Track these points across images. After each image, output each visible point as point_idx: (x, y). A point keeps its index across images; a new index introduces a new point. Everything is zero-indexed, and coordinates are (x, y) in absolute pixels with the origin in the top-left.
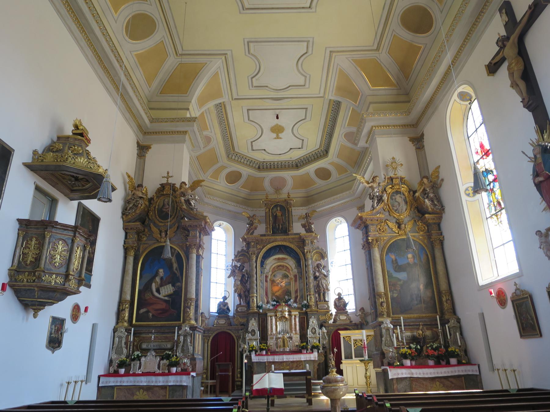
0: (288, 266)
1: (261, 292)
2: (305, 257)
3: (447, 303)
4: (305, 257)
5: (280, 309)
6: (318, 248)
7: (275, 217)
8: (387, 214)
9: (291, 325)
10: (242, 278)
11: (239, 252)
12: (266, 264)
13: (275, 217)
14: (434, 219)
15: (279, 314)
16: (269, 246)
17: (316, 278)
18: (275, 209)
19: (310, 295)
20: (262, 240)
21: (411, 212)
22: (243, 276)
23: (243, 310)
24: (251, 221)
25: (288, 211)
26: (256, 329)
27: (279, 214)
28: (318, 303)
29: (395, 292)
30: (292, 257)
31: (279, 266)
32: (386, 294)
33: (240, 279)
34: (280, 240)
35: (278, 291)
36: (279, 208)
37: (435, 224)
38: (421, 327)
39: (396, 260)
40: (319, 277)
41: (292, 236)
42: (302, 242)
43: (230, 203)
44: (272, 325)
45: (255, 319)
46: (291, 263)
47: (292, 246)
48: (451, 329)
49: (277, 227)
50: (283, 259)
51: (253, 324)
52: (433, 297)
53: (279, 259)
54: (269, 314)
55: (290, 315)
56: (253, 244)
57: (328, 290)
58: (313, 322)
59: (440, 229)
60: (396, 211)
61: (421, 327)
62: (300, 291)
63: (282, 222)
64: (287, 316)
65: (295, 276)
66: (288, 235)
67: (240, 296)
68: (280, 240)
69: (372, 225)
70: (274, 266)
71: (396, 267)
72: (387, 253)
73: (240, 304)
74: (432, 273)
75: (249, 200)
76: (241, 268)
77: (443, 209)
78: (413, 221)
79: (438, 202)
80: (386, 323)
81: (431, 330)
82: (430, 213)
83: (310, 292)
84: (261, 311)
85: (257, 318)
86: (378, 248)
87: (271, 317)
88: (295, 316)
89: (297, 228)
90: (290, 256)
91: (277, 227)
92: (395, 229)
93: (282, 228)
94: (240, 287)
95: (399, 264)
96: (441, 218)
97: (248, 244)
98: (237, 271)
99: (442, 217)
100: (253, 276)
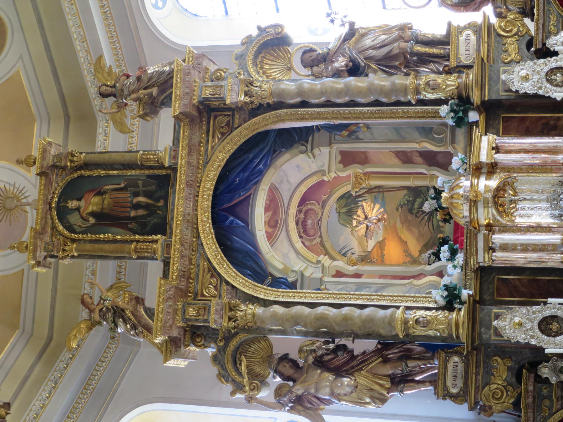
0: (303, 189)
1: (395, 292)
2: (271, 107)
4: (271, 107)
5: (462, 213)
6: (241, 57)
7: (104, 219)
9: (531, 168)
10: (330, 370)
11: (223, 376)
12: (286, 270)
13: (104, 219)
15: (484, 216)
16: (212, 249)
17: (354, 70)
18: (74, 219)
19: (417, 91)
20: (186, 275)
22: (320, 363)
23: (461, 367)
24: (103, 315)
25: (86, 166)
26: (539, 312)
27: (92, 204)
28: (453, 63)
30: (267, 166)
31: (302, 225)
33: (331, 377)
34: (192, 205)
35: (404, 243)
36: (72, 204)
40: (352, 60)
41: (182, 152)
42: (208, 114)
43: (36, 404)
44: (526, 248)
45: (497, 317)
46: (291, 172)
47: (220, 158)
49: (141, 212)
50: (273, 205)
51: (517, 324)
53: (273, 224)
54: (482, 258)
55: (492, 168)
56: (192, 312)
57: (403, 28)
58: (526, 78)
62: (403, 140)
63: (127, 195)
64: (494, 183)
65: (348, 159)
66: (174, 169)
67: (400, 382)
68: (192, 205)
70: (299, 245)
73: (432, 381)
75: (50, 339)
76: (288, 370)
83: (405, 90)
84: (465, 293)
85: (495, 310)
87: (493, 250)
88: (497, 149)
89: (159, 137)
90: (261, 173)
91: (141, 212)
93: (147, 194)
94: (362, 379)
97: (196, 333)
98: (299, 390)
100: (322, 318)
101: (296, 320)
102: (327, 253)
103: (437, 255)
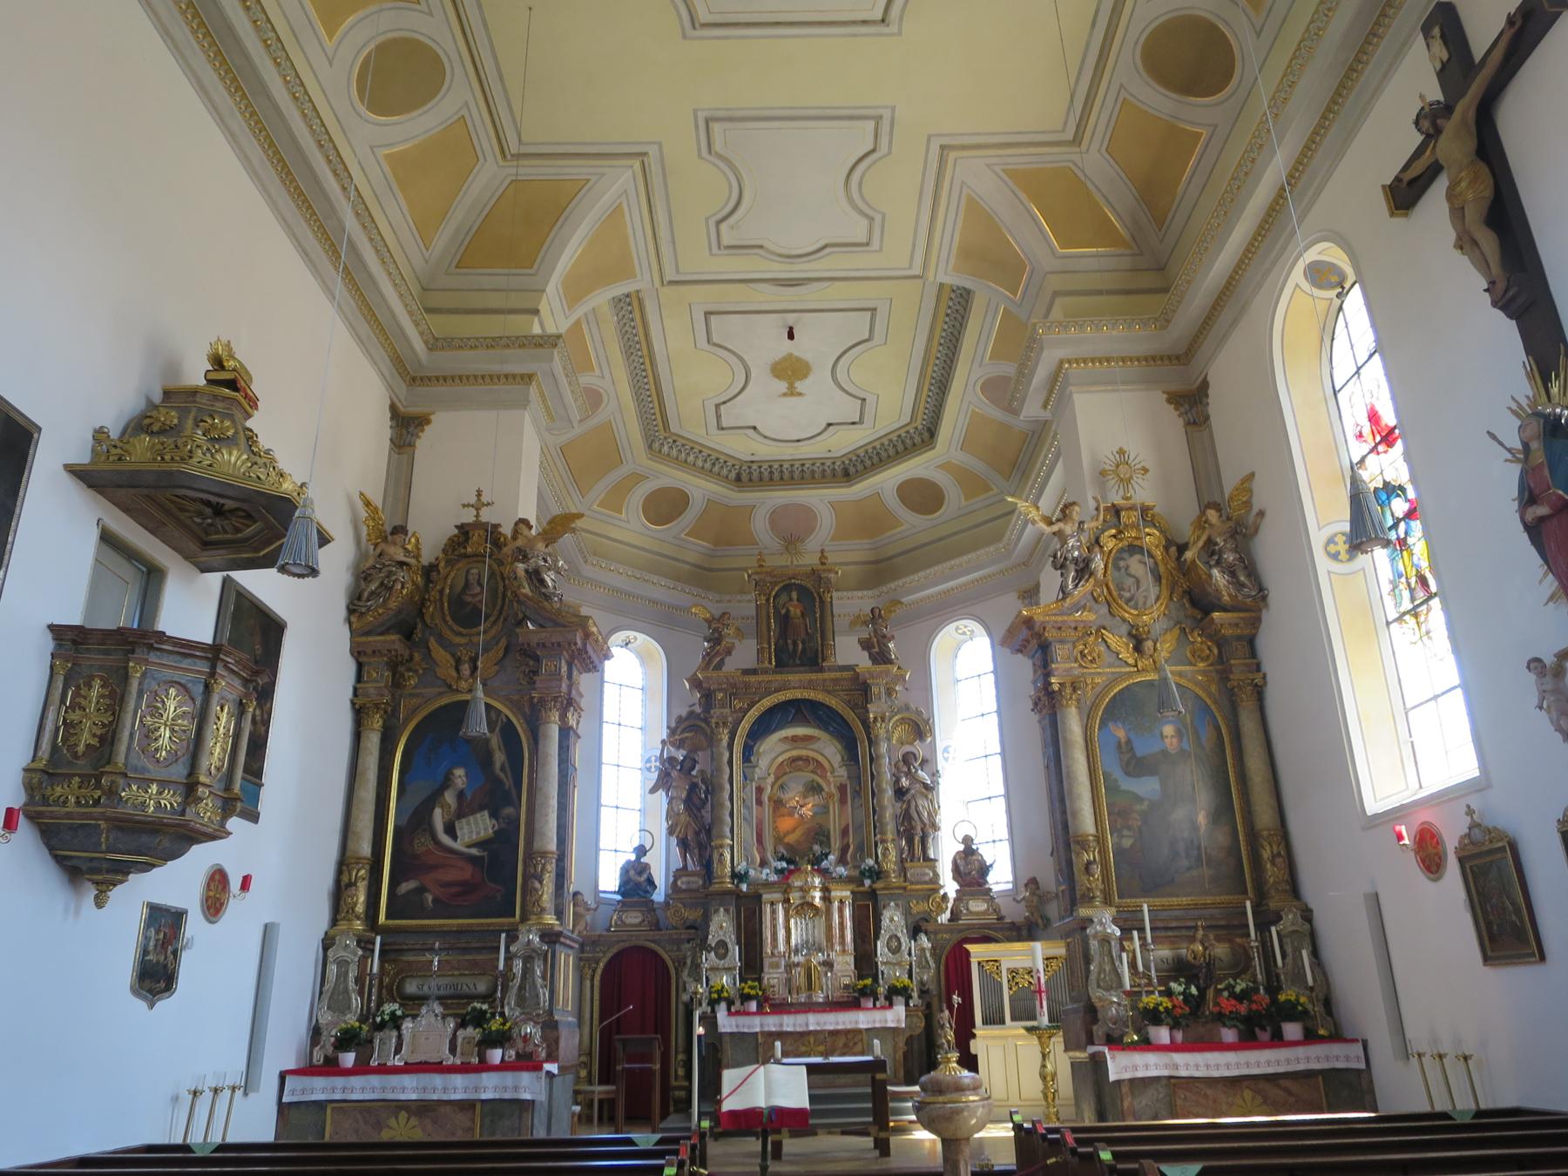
0: (820, 758)
1: (745, 833)
2: (868, 734)
3: (1273, 864)
4: (868, 734)
5: (797, 882)
6: (907, 708)
7: (785, 620)
8: (1105, 610)
9: (829, 927)
10: (689, 795)
11: (680, 720)
12: (759, 754)
13: (785, 620)
14: (1237, 625)
15: (795, 898)
16: (767, 703)
17: (900, 793)
18: (783, 598)
19: (883, 841)
20: (747, 686)
21: (1172, 606)
22: (693, 788)
23: (694, 886)
24: (715, 630)
25: (822, 602)
26: (731, 939)
27: (795, 610)
28: (908, 865)
29: (1125, 832)
30: (831, 733)
31: (794, 760)
32: (1100, 839)
33: (684, 795)
34: (798, 685)
35: (793, 831)
36: (794, 595)
37: (1239, 638)
38: (1201, 932)
39: (1129, 741)
40: (908, 790)
41: (833, 675)
42: (861, 690)
43: (655, 579)
44: (774, 927)
45: (727, 911)
46: (829, 750)
47: (833, 702)
48: (1287, 940)
49: (791, 647)
50: (808, 739)
51: (722, 926)
52: (1234, 849)
53: (794, 739)
55: (827, 899)
57: (935, 827)
58: (892, 920)
59: (1253, 653)
60: (1128, 601)
61: (1201, 932)
62: (855, 830)
63: (803, 634)
64: (817, 902)
65: (842, 788)
66: (821, 670)
67: (684, 845)
68: (798, 685)
69: (1062, 642)
70: (780, 759)
71: (1128, 763)
72: (1103, 723)
73: (685, 867)
74: (1232, 779)
75: (711, 570)
76: (688, 764)
77: (1264, 598)
78: (1176, 631)
79: (1249, 576)
80: (1101, 923)
81: (1230, 941)
82: (1225, 609)
83: (883, 833)
84: (744, 887)
85: (732, 909)
86: (1078, 707)
87: (772, 904)
88: (841, 902)
89: (848, 651)
90: (826, 730)
91: (791, 647)
92: (1127, 654)
93: (804, 651)
94: (684, 818)
95: (1139, 754)
96: (1256, 622)
97: (708, 697)
98: (674, 774)
99: (1259, 620)
100: (722, 788)
101: (719, 770)
102: (777, 779)
103: (782, 859)
